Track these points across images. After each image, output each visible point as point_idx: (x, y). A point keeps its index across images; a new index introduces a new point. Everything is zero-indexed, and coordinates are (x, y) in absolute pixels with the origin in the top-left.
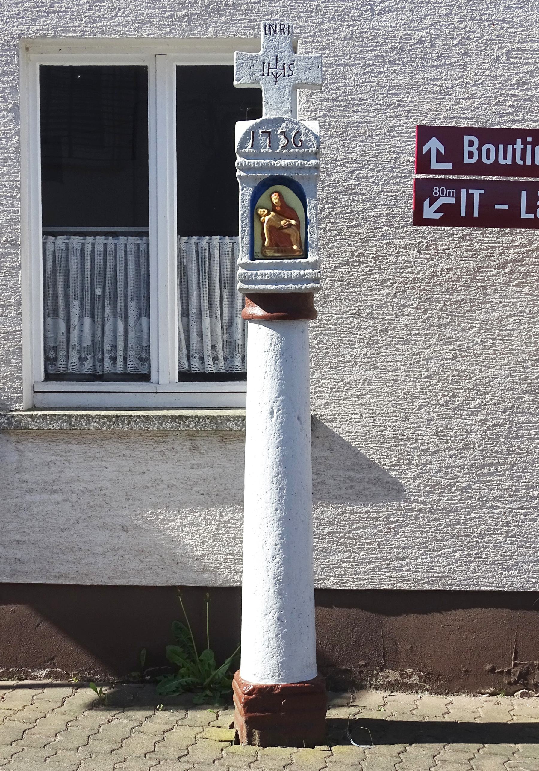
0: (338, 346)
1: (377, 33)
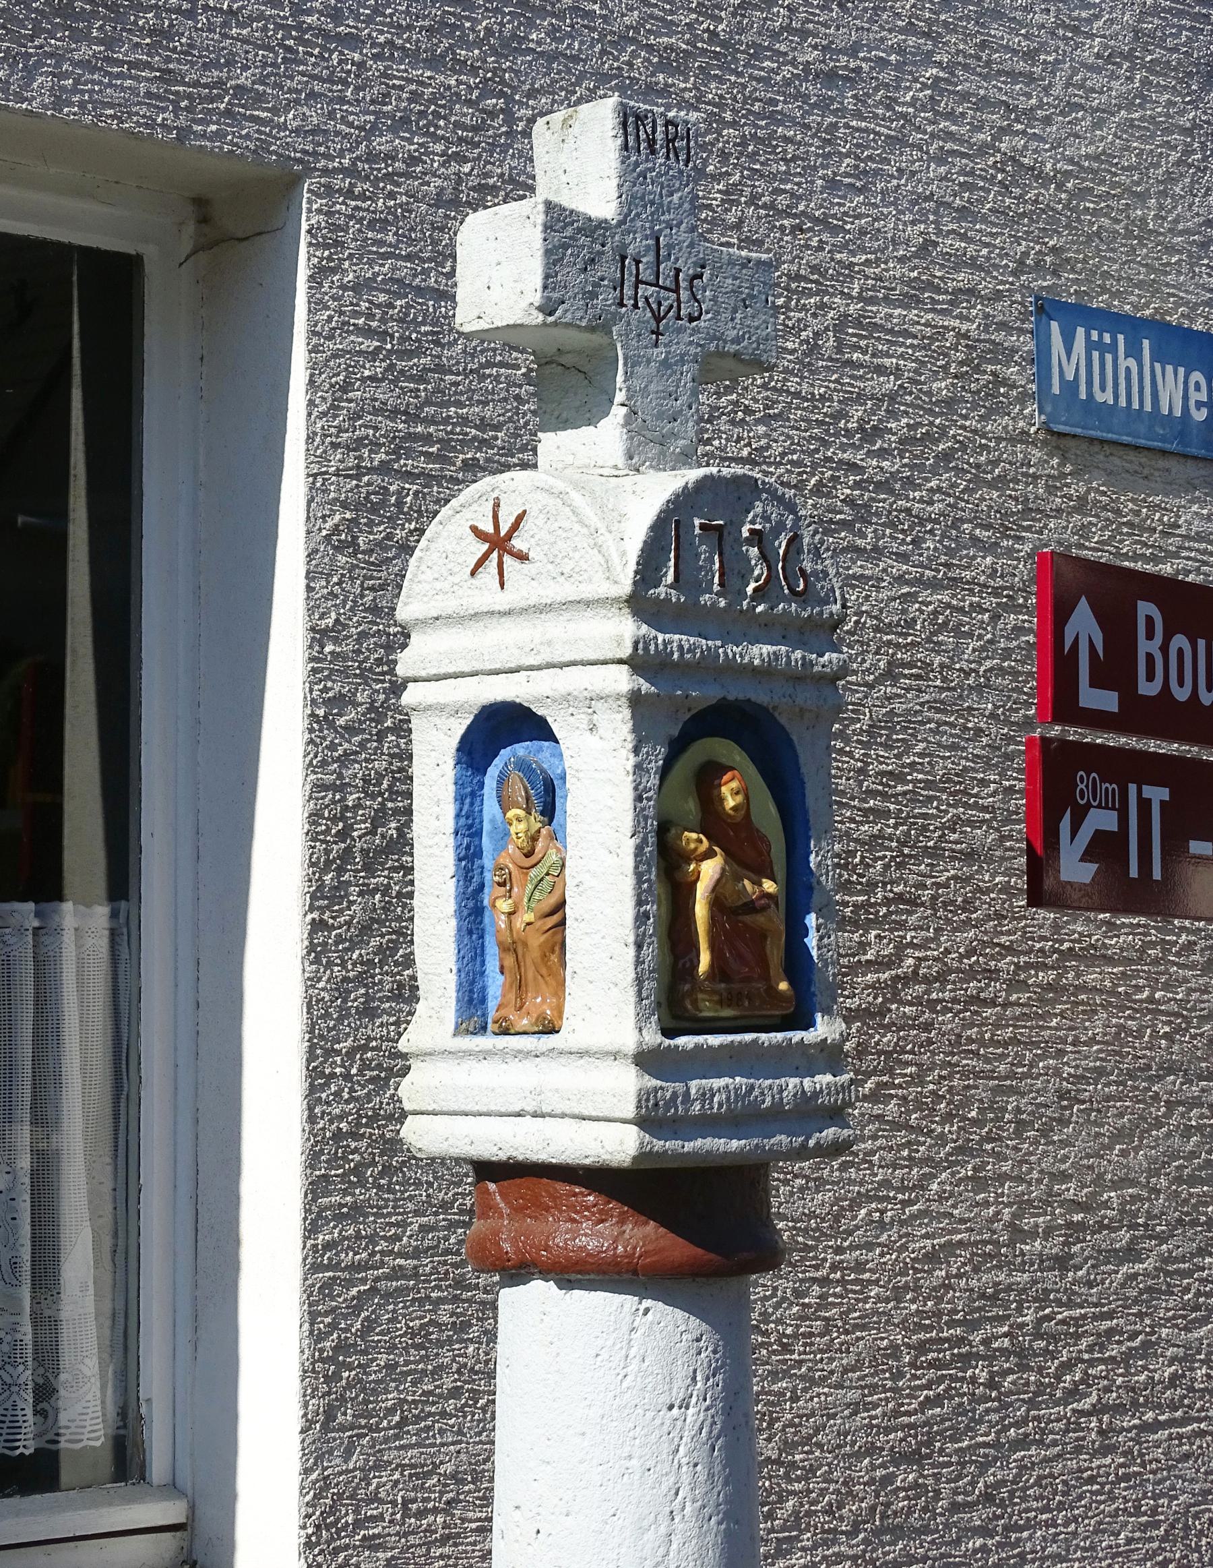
0: (421, 1338)
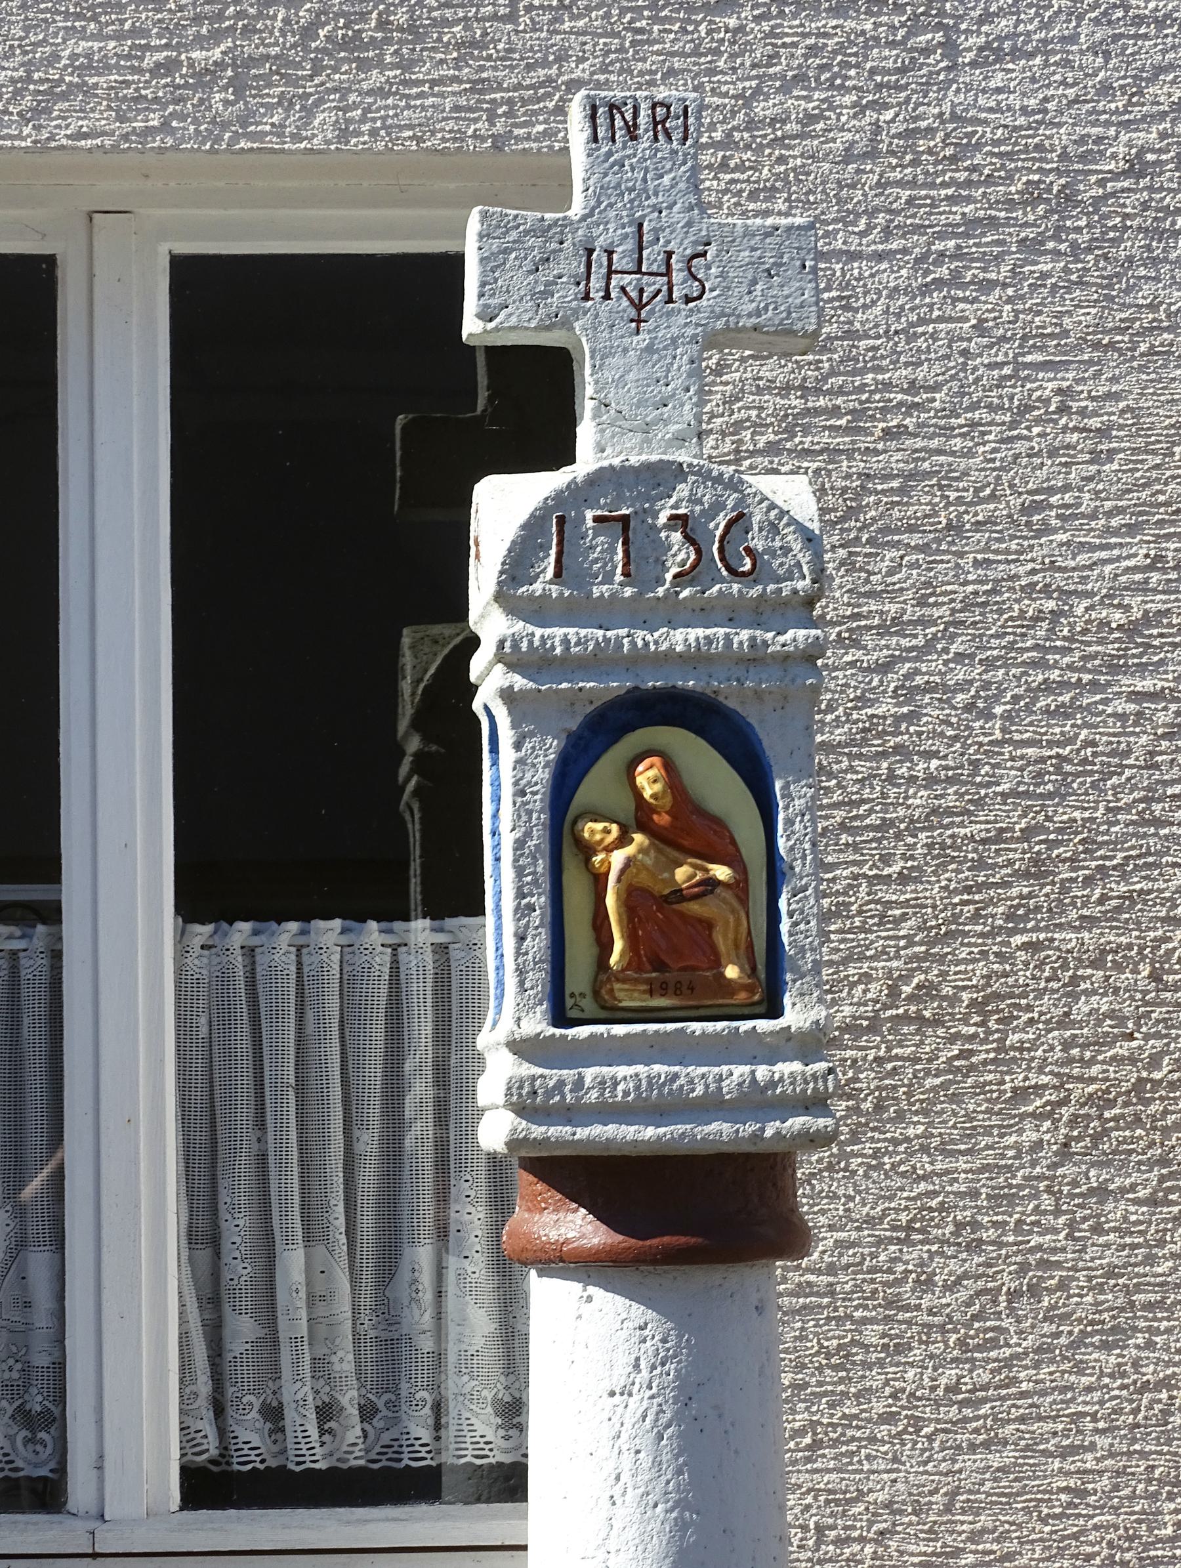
1: (970, 135)
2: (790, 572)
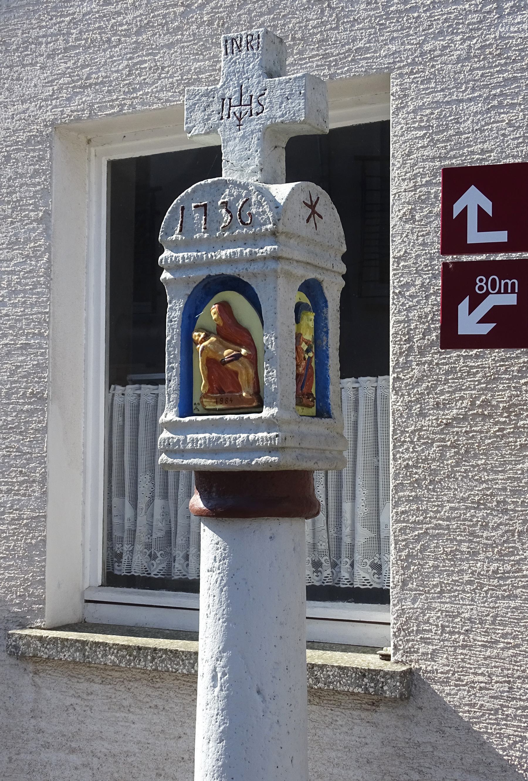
2: (265, 221)
